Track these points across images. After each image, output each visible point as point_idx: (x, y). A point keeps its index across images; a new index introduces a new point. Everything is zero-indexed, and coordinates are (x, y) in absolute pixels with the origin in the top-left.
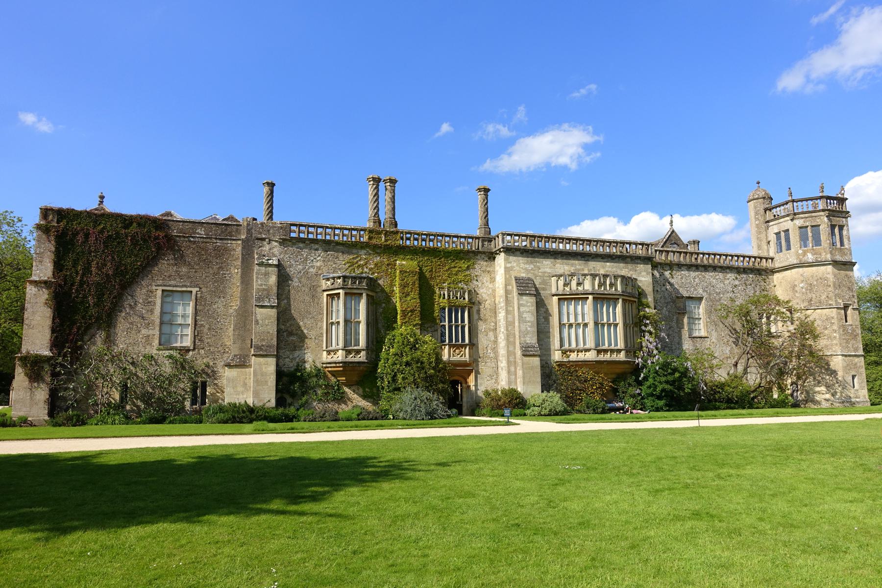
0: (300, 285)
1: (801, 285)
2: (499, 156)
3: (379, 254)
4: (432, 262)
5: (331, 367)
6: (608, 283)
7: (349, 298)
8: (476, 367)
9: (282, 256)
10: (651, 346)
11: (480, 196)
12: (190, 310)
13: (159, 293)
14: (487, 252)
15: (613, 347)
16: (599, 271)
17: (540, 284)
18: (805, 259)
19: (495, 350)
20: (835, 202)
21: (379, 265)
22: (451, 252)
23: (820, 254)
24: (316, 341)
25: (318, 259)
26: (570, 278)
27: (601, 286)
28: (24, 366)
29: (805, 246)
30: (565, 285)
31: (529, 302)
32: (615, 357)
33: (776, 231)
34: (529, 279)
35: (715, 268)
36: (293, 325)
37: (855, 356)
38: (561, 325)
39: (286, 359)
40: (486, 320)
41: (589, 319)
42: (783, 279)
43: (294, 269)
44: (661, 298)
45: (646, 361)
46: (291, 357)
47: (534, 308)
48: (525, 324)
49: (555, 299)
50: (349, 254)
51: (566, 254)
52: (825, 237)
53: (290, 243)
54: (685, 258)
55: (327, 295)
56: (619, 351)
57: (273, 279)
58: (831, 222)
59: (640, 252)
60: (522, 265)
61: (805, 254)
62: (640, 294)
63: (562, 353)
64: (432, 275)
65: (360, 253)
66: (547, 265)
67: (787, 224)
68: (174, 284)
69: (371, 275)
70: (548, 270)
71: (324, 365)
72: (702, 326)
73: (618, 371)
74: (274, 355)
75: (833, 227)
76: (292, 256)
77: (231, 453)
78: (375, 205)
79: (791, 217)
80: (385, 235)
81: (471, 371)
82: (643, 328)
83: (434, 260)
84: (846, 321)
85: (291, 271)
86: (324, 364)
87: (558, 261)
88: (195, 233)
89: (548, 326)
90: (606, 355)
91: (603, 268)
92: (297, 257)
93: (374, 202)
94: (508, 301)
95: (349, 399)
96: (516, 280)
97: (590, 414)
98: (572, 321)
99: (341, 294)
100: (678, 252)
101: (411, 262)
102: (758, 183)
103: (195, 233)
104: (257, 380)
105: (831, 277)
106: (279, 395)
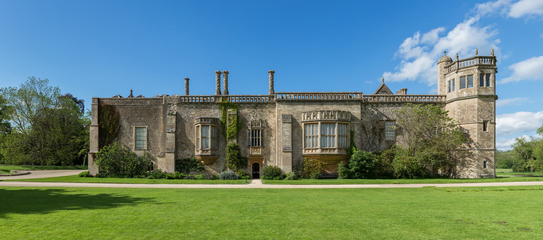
1: (458, 111)
2: (399, 48)
7: (204, 128)
12: (145, 134)
13: (134, 128)
16: (329, 109)
20: (489, 59)
23: (471, 92)
27: (326, 117)
31: (288, 127)
32: (332, 153)
38: (305, 137)
42: (450, 108)
43: (184, 115)
44: (370, 121)
47: (290, 129)
48: (285, 137)
49: (303, 124)
52: (475, 81)
53: (181, 105)
54: (343, 96)
56: (335, 149)
57: (174, 121)
60: (286, 108)
61: (462, 92)
66: (300, 108)
68: (140, 125)
74: (173, 152)
77: (487, 4)
79: (456, 71)
96: (282, 115)
100: (386, 96)
102: (445, 52)
104: (167, 162)
105: (476, 105)
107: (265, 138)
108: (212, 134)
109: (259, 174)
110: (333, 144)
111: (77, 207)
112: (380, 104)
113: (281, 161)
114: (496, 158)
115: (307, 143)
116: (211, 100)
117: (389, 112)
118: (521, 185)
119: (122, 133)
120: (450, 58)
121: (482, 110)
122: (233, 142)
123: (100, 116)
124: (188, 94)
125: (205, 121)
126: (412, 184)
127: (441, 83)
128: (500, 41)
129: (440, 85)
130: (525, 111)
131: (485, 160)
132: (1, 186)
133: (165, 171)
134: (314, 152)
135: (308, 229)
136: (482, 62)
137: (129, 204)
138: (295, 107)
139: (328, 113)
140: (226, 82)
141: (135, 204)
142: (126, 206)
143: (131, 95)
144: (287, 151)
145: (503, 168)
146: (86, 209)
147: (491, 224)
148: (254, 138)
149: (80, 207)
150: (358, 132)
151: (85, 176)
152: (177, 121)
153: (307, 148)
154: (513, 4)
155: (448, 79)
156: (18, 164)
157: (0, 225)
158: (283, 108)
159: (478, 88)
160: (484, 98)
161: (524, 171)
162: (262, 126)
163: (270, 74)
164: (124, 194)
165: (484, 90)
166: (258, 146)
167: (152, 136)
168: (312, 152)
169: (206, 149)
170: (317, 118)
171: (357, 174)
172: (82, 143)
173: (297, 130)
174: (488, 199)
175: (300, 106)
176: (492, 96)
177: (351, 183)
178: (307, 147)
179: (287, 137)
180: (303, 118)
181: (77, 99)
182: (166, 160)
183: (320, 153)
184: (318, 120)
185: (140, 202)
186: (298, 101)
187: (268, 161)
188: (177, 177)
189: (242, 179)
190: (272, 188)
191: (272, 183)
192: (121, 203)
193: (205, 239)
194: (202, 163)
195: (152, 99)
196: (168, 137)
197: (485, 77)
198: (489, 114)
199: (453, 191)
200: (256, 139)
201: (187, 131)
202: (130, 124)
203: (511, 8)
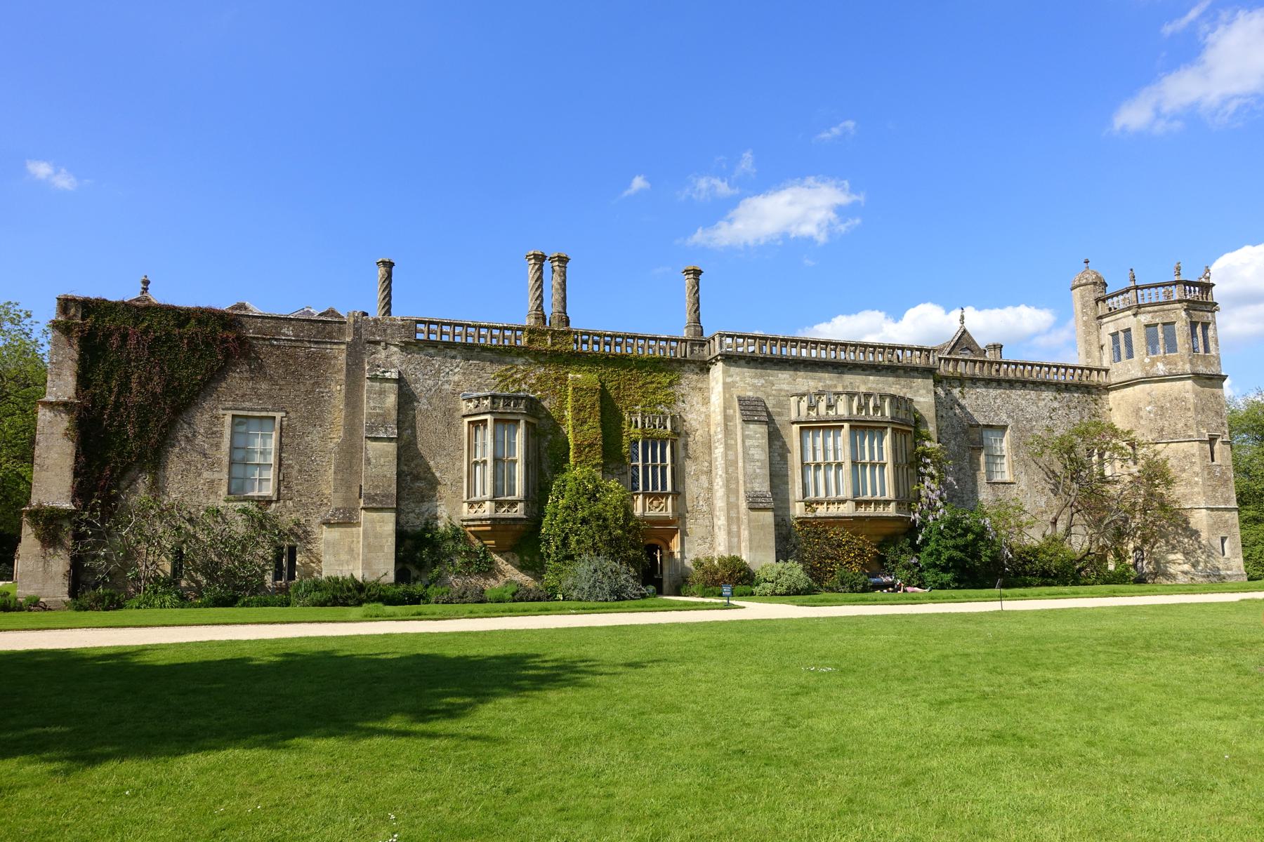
0: (430, 408)
1: (1148, 409)
2: (715, 223)
3: (543, 364)
4: (619, 375)
5: (474, 526)
6: (871, 405)
8: (682, 525)
9: (404, 367)
10: (933, 496)
11: (688, 281)
13: (228, 419)
14: (698, 361)
15: (878, 497)
16: (858, 388)
17: (774, 406)
18: (1153, 371)
19: (709, 501)
20: (1197, 289)
21: (544, 379)
22: (646, 361)
23: (1176, 364)
24: (453, 488)
25: (456, 370)
27: (862, 409)
28: (35, 524)
29: (1154, 352)
30: (810, 408)
31: (758, 433)
32: (881, 511)
33: (1113, 331)
34: (758, 400)
35: (1024, 384)
36: (421, 465)
37: (1226, 509)
38: (804, 466)
39: (410, 514)
40: (696, 459)
41: (845, 456)
42: (1121, 400)
43: (422, 385)
45: (926, 517)
46: (417, 511)
48: (752, 464)
49: (796, 427)
50: (501, 364)
51: (810, 364)
52: (1182, 340)
53: (415, 348)
54: (981, 369)
55: (469, 422)
56: (887, 503)
57: (391, 400)
58: (1191, 317)
59: (918, 360)
60: (748, 380)
61: (1153, 363)
62: (917, 421)
63: (806, 505)
64: (619, 394)
65: (516, 363)
66: (783, 380)
67: (1127, 320)
68: (250, 407)
69: (532, 394)
70: (786, 387)
71: (465, 523)
72: (1005, 467)
73: (885, 531)
74: (392, 508)
75: (1193, 325)
76: (418, 367)
77: (331, 649)
78: (538, 293)
79: (1134, 311)
80: (552, 336)
81: (675, 531)
82: (922, 469)
83: (622, 373)
84: (1213, 460)
85: (417, 389)
86: (465, 521)
87: (800, 373)
88: (279, 333)
89: (785, 466)
90: (868, 509)
91: (865, 383)
92: (426, 368)
93: (537, 290)
94: (728, 431)
95: (500, 572)
96: (739, 400)
97: (845, 592)
98: (820, 459)
99: (489, 421)
100: (971, 361)
101: (589, 376)
102: (1087, 262)
103: (279, 333)
105: (1191, 397)
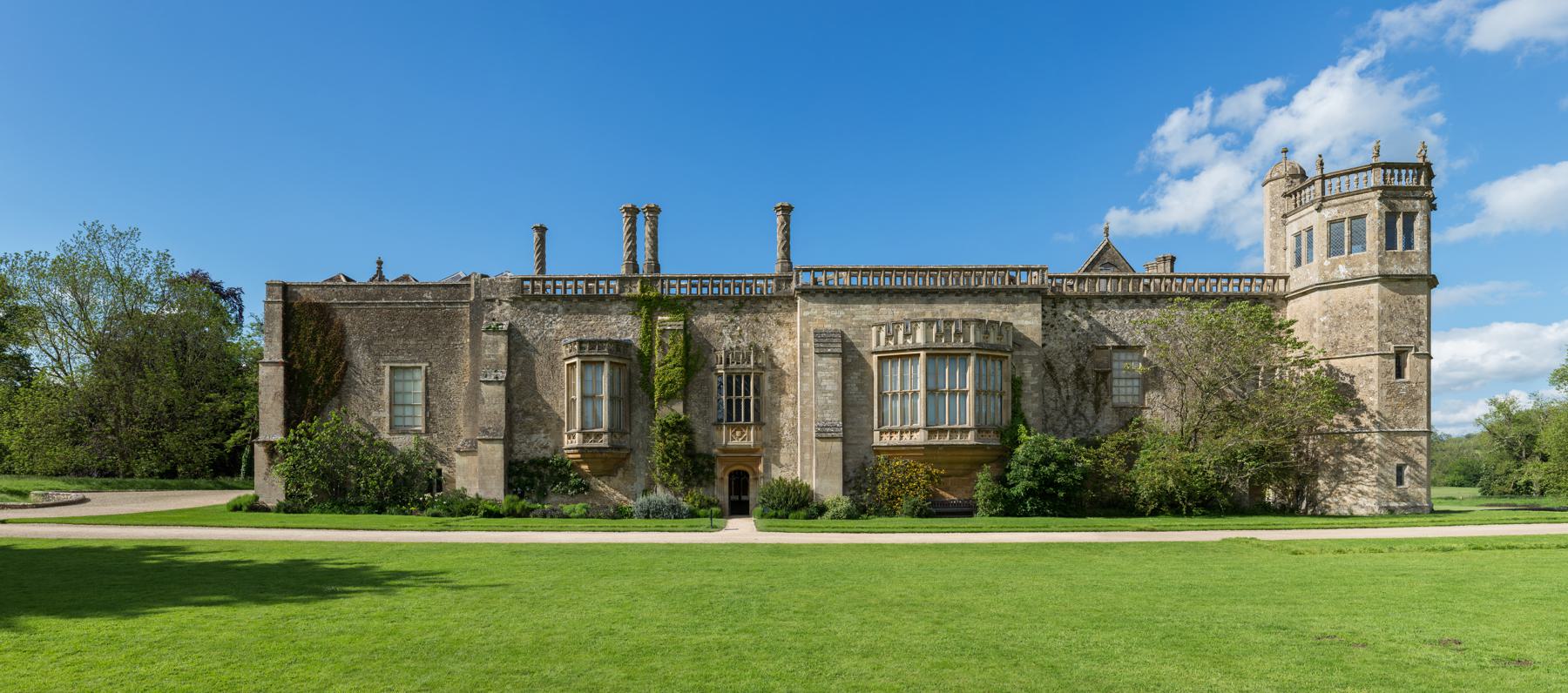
1: (1322, 320)
2: (1152, 138)
7: (590, 371)
13: (387, 370)
16: (950, 314)
20: (1411, 172)
23: (1361, 265)
26: (914, 325)
27: (941, 337)
31: (832, 365)
32: (958, 441)
38: (882, 396)
42: (1298, 311)
43: (531, 333)
47: (838, 373)
48: (824, 395)
49: (875, 357)
52: (1372, 235)
53: (523, 303)
54: (990, 278)
56: (966, 431)
57: (502, 348)
60: (827, 312)
61: (1334, 267)
66: (865, 312)
68: (403, 360)
74: (500, 439)
77: (1407, 10)
79: (1316, 205)
96: (815, 333)
100: (1113, 277)
102: (1286, 151)
105: (1375, 304)
106: (744, 498)
107: (765, 397)
108: (613, 386)
109: (748, 502)
110: (962, 414)
111: (222, 598)
112: (1096, 300)
113: (811, 464)
114: (1433, 457)
115: (887, 412)
116: (609, 288)
117: (1124, 322)
118: (1503, 534)
119: (354, 383)
120: (1301, 168)
121: (1391, 317)
122: (673, 410)
123: (287, 336)
124: (542, 271)
125: (593, 348)
126: (1189, 532)
127: (1274, 241)
128: (1445, 119)
129: (1272, 245)
130: (1517, 321)
131: (1400, 461)
132: (2, 538)
133: (477, 495)
134: (907, 438)
135: (891, 662)
136: (1392, 179)
137: (373, 589)
138: (852, 309)
139: (948, 328)
140: (652, 238)
141: (391, 590)
142: (364, 593)
143: (380, 275)
144: (829, 435)
145: (1452, 485)
146: (248, 603)
147: (1417, 647)
148: (734, 397)
149: (231, 599)
150: (1035, 381)
151: (245, 508)
152: (512, 348)
153: (888, 427)
154: (1482, 11)
155: (1293, 228)
156: (52, 474)
157: (1, 649)
158: (816, 312)
159: (1379, 254)
160: (1397, 283)
161: (1512, 493)
162: (755, 364)
163: (780, 213)
164: (358, 560)
165: (1397, 259)
166: (745, 420)
167: (439, 394)
168: (901, 439)
169: (596, 430)
170: (914, 342)
171: (1030, 502)
172: (238, 413)
173: (859, 374)
174: (1409, 575)
175: (866, 306)
176: (1420, 277)
177: (1012, 529)
178: (887, 424)
179: (829, 395)
180: (875, 341)
181: (223, 285)
182: (481, 462)
183: (925, 441)
184: (918, 347)
185: (404, 582)
186: (861, 293)
187: (773, 466)
188: (510, 511)
189: (699, 517)
190: (786, 542)
191: (786, 529)
192: (348, 586)
193: (591, 692)
194: (582, 470)
195: (440, 285)
196: (484, 394)
197: (1399, 223)
198: (1413, 330)
199: (1307, 551)
200: (739, 401)
201: (539, 379)
202: (377, 357)
203: (1475, 23)
